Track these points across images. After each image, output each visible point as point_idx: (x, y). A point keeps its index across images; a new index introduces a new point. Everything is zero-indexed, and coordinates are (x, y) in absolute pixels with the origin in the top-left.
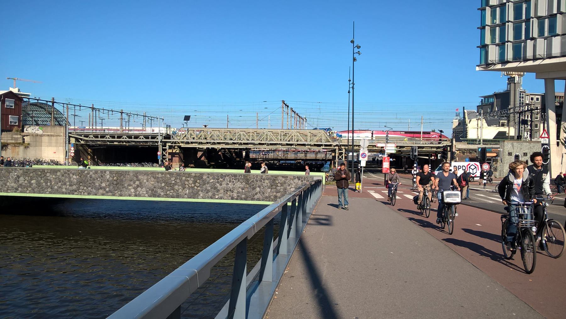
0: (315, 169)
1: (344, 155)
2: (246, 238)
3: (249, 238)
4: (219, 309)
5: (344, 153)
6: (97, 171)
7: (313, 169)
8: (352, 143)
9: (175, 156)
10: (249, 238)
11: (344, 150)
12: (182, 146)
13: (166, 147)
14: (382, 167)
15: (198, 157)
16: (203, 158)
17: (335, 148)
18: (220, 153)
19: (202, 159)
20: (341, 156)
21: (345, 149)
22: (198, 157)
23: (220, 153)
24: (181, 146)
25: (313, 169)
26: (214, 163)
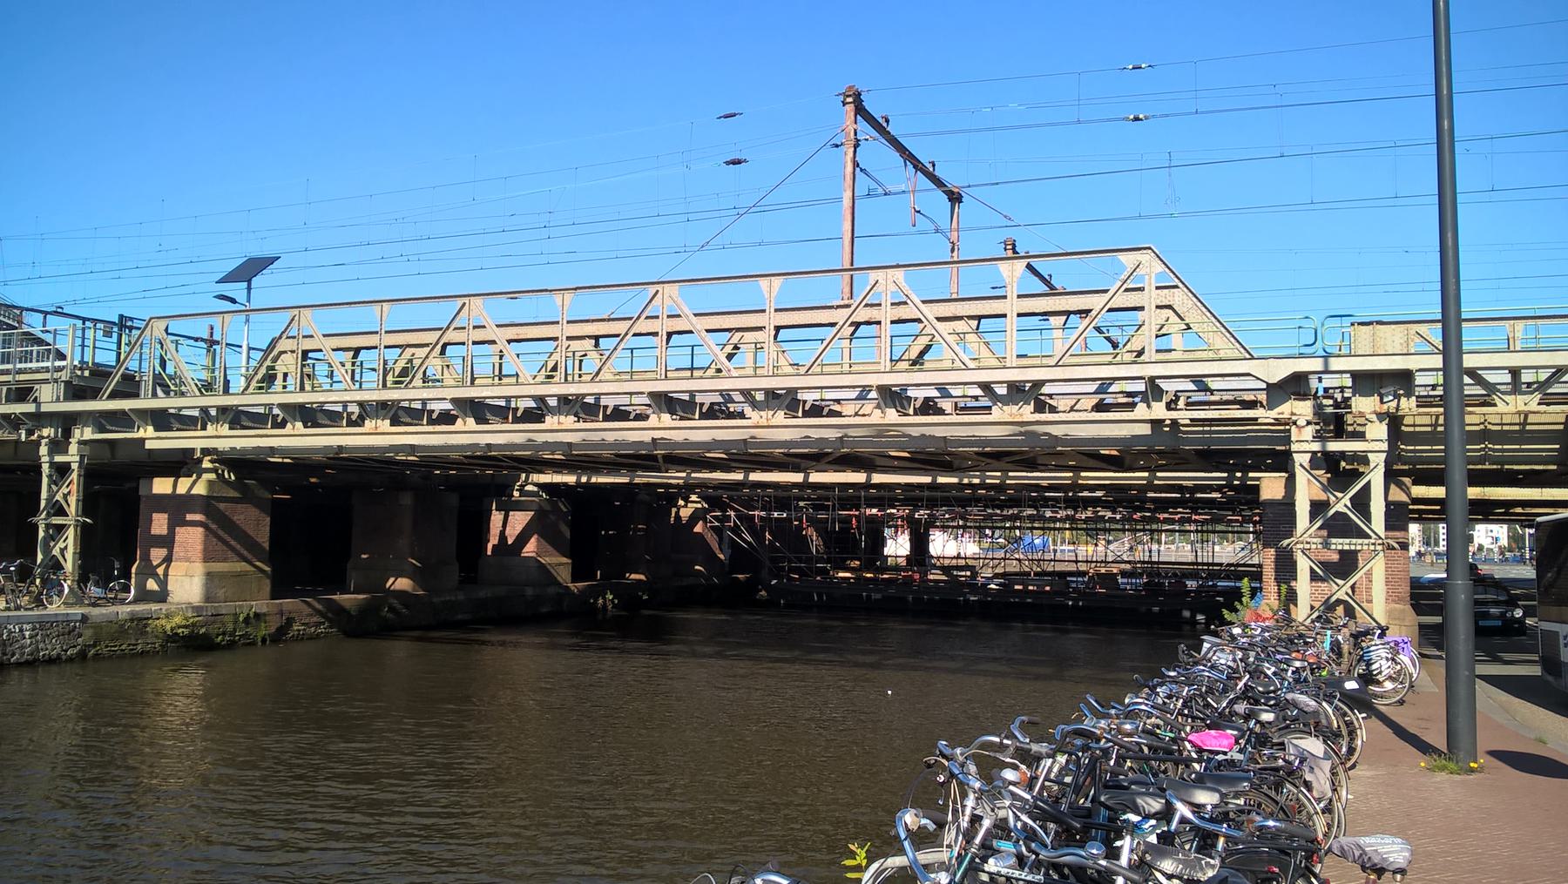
0: (1200, 617)
1: (1376, 478)
2: (1296, 605)
3: (1292, 606)
4: (1352, 504)
5: (1378, 461)
6: (141, 619)
7: (1187, 614)
8: (1445, 353)
9: (189, 517)
10: (1292, 606)
11: (1378, 431)
12: (149, 445)
13: (65, 452)
14: (209, 576)
15: (510, 543)
16: (530, 548)
17: (1286, 409)
18: (698, 528)
19: (524, 550)
20: (1344, 490)
21: (1381, 416)
22: (510, 543)
23: (698, 528)
24: (143, 440)
25: (1187, 614)
26: (642, 577)
